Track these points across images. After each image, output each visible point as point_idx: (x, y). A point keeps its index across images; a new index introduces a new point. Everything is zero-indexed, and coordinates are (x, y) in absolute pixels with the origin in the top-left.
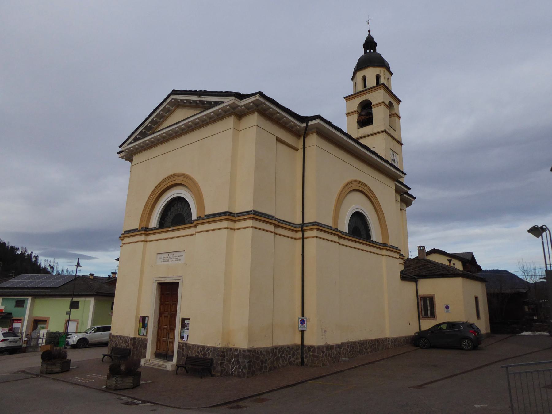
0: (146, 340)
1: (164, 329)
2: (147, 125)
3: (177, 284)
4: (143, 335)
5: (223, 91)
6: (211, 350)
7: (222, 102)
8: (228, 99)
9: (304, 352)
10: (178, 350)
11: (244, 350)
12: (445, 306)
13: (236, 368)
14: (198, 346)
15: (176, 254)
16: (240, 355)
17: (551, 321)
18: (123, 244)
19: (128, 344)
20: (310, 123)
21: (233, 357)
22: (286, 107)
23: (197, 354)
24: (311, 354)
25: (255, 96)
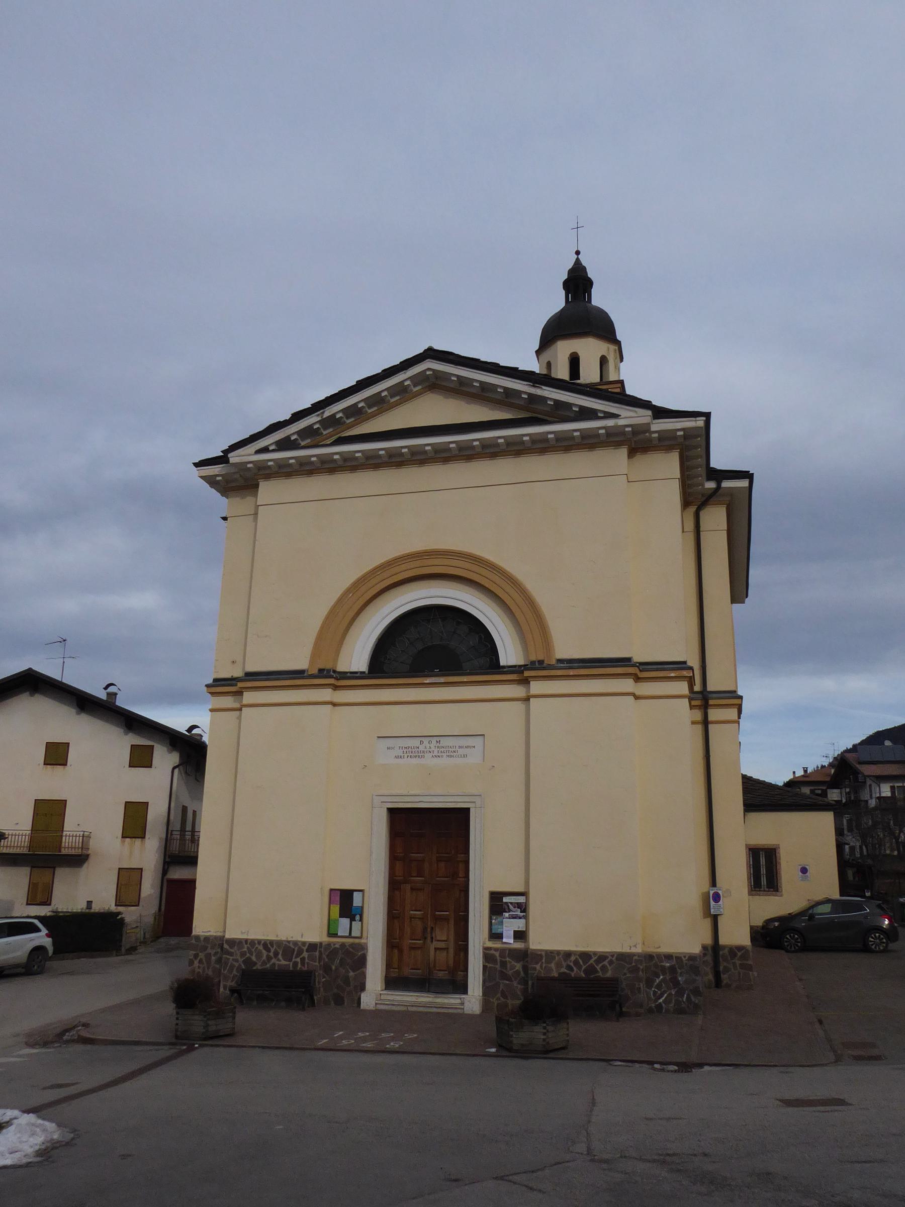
0: (363, 948)
1: (411, 918)
3: (464, 814)
4: (350, 936)
5: (483, 359)
7: (616, 416)
8: (636, 412)
9: (721, 959)
10: (485, 967)
11: (689, 957)
12: (800, 867)
13: (670, 994)
15: (445, 742)
17: (902, 900)
19: (298, 960)
20: (726, 484)
21: (732, 967)
23: (563, 970)
24: (738, 962)
25: (694, 419)
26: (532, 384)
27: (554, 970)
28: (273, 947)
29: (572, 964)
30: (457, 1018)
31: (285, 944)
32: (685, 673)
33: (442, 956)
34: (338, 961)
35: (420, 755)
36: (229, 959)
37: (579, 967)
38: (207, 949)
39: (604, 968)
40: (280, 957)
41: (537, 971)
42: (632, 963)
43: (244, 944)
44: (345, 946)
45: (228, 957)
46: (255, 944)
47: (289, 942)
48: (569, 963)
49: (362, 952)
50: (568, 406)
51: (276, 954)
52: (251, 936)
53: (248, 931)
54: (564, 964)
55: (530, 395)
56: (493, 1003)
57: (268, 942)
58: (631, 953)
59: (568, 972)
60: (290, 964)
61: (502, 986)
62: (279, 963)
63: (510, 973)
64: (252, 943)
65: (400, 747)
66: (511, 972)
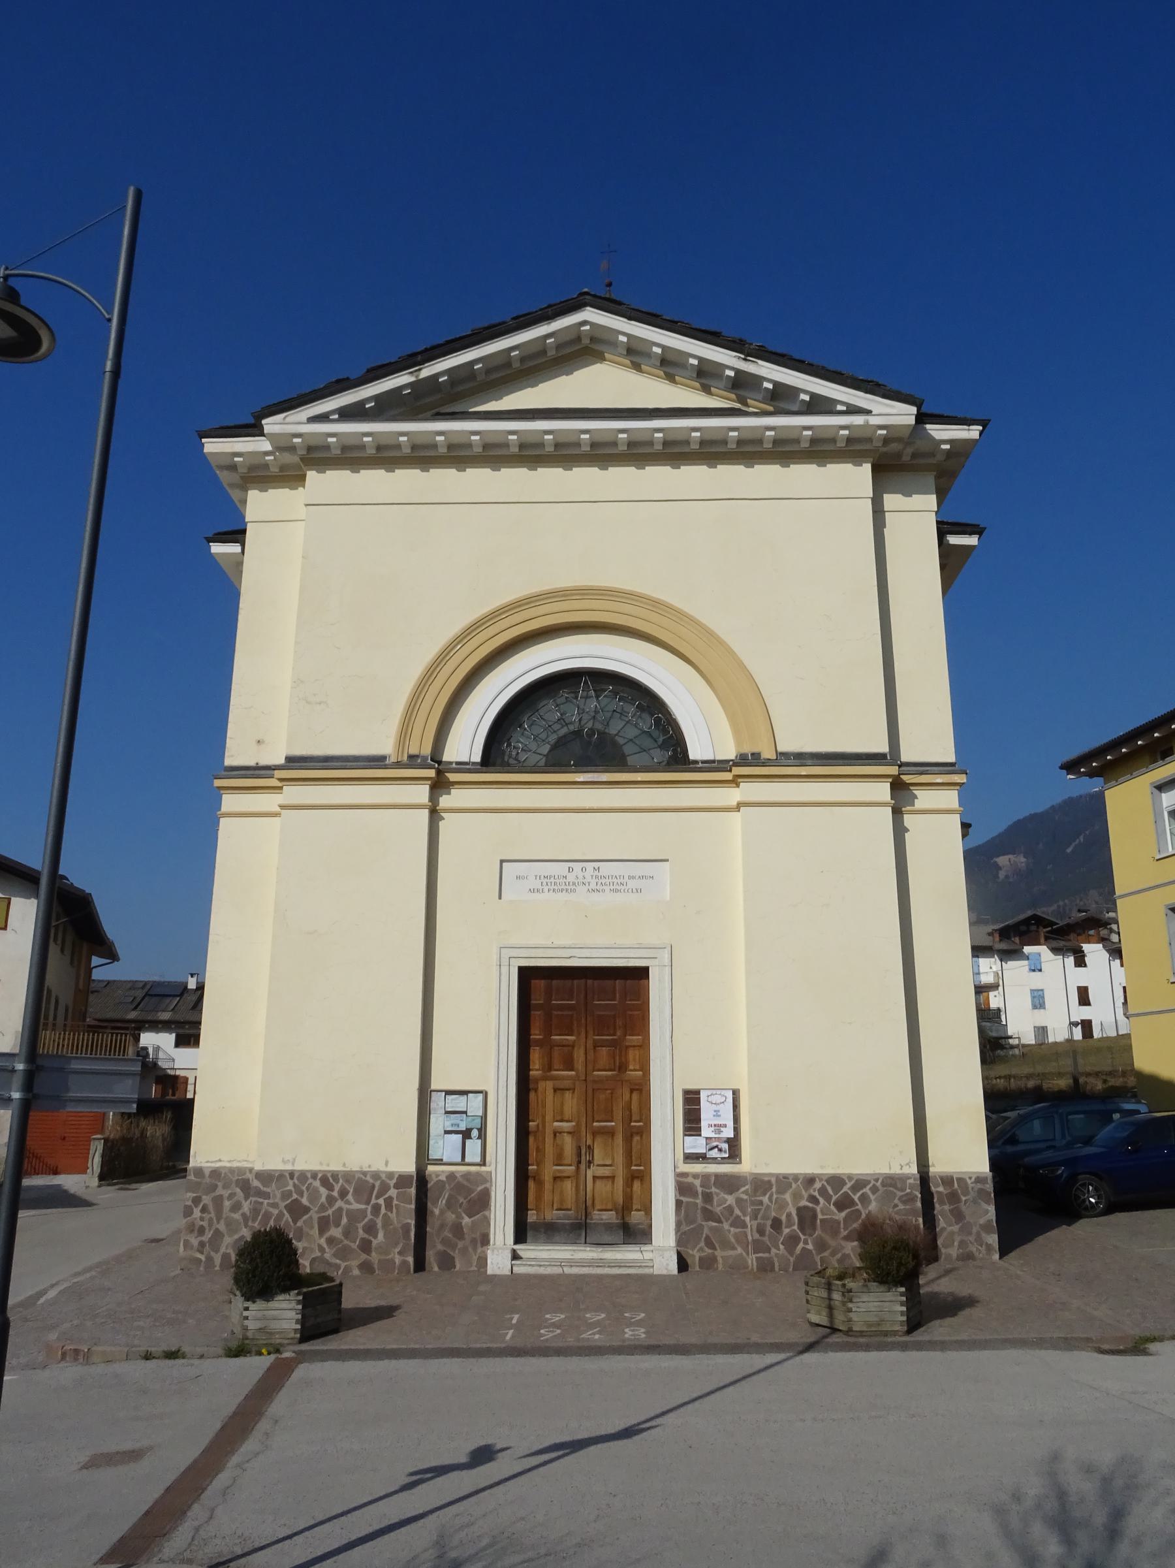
0: (486, 1179)
2: (436, 377)
4: (463, 1162)
6: (874, 1185)
10: (679, 1204)
14: (810, 1180)
16: (966, 1193)
18: (282, 807)
19: (381, 1201)
22: (564, 376)
26: (743, 356)
27: (790, 1203)
28: (337, 1183)
29: (816, 1194)
30: (645, 1282)
31: (359, 1178)
32: (956, 778)
33: (603, 1188)
34: (444, 1202)
35: (569, 888)
36: (262, 1203)
37: (828, 1198)
38: (216, 1189)
39: (864, 1199)
40: (350, 1197)
41: (765, 1206)
42: (906, 1189)
43: (289, 1178)
44: (456, 1177)
45: (261, 1200)
46: (307, 1179)
47: (365, 1173)
48: (812, 1191)
49: (483, 1187)
50: (794, 391)
51: (343, 1194)
52: (301, 1166)
53: (294, 1160)
54: (806, 1195)
55: (738, 372)
56: (694, 1256)
57: (329, 1175)
58: (903, 1174)
59: (811, 1205)
60: (367, 1208)
61: (706, 1231)
62: (348, 1206)
63: (718, 1210)
64: (303, 1176)
65: (536, 876)
66: (719, 1208)
